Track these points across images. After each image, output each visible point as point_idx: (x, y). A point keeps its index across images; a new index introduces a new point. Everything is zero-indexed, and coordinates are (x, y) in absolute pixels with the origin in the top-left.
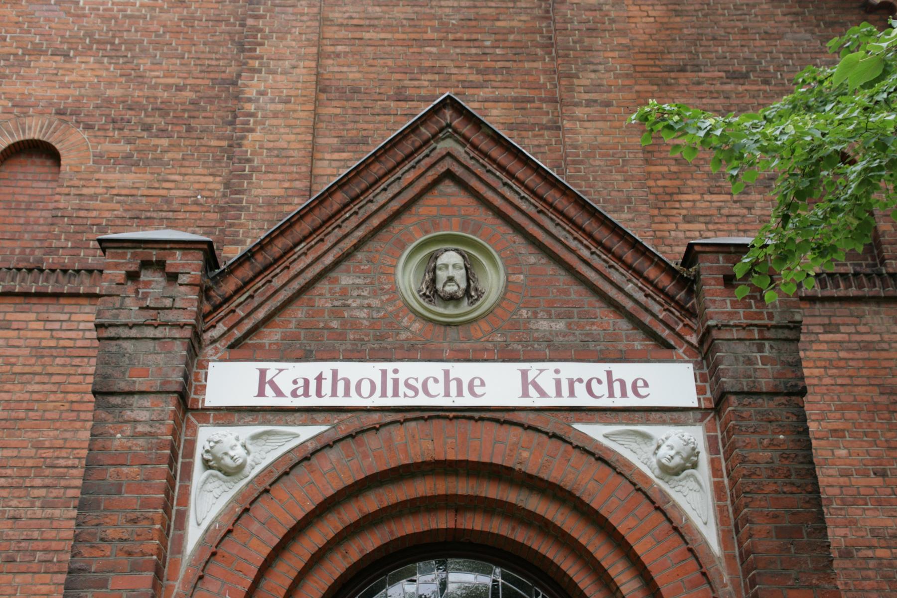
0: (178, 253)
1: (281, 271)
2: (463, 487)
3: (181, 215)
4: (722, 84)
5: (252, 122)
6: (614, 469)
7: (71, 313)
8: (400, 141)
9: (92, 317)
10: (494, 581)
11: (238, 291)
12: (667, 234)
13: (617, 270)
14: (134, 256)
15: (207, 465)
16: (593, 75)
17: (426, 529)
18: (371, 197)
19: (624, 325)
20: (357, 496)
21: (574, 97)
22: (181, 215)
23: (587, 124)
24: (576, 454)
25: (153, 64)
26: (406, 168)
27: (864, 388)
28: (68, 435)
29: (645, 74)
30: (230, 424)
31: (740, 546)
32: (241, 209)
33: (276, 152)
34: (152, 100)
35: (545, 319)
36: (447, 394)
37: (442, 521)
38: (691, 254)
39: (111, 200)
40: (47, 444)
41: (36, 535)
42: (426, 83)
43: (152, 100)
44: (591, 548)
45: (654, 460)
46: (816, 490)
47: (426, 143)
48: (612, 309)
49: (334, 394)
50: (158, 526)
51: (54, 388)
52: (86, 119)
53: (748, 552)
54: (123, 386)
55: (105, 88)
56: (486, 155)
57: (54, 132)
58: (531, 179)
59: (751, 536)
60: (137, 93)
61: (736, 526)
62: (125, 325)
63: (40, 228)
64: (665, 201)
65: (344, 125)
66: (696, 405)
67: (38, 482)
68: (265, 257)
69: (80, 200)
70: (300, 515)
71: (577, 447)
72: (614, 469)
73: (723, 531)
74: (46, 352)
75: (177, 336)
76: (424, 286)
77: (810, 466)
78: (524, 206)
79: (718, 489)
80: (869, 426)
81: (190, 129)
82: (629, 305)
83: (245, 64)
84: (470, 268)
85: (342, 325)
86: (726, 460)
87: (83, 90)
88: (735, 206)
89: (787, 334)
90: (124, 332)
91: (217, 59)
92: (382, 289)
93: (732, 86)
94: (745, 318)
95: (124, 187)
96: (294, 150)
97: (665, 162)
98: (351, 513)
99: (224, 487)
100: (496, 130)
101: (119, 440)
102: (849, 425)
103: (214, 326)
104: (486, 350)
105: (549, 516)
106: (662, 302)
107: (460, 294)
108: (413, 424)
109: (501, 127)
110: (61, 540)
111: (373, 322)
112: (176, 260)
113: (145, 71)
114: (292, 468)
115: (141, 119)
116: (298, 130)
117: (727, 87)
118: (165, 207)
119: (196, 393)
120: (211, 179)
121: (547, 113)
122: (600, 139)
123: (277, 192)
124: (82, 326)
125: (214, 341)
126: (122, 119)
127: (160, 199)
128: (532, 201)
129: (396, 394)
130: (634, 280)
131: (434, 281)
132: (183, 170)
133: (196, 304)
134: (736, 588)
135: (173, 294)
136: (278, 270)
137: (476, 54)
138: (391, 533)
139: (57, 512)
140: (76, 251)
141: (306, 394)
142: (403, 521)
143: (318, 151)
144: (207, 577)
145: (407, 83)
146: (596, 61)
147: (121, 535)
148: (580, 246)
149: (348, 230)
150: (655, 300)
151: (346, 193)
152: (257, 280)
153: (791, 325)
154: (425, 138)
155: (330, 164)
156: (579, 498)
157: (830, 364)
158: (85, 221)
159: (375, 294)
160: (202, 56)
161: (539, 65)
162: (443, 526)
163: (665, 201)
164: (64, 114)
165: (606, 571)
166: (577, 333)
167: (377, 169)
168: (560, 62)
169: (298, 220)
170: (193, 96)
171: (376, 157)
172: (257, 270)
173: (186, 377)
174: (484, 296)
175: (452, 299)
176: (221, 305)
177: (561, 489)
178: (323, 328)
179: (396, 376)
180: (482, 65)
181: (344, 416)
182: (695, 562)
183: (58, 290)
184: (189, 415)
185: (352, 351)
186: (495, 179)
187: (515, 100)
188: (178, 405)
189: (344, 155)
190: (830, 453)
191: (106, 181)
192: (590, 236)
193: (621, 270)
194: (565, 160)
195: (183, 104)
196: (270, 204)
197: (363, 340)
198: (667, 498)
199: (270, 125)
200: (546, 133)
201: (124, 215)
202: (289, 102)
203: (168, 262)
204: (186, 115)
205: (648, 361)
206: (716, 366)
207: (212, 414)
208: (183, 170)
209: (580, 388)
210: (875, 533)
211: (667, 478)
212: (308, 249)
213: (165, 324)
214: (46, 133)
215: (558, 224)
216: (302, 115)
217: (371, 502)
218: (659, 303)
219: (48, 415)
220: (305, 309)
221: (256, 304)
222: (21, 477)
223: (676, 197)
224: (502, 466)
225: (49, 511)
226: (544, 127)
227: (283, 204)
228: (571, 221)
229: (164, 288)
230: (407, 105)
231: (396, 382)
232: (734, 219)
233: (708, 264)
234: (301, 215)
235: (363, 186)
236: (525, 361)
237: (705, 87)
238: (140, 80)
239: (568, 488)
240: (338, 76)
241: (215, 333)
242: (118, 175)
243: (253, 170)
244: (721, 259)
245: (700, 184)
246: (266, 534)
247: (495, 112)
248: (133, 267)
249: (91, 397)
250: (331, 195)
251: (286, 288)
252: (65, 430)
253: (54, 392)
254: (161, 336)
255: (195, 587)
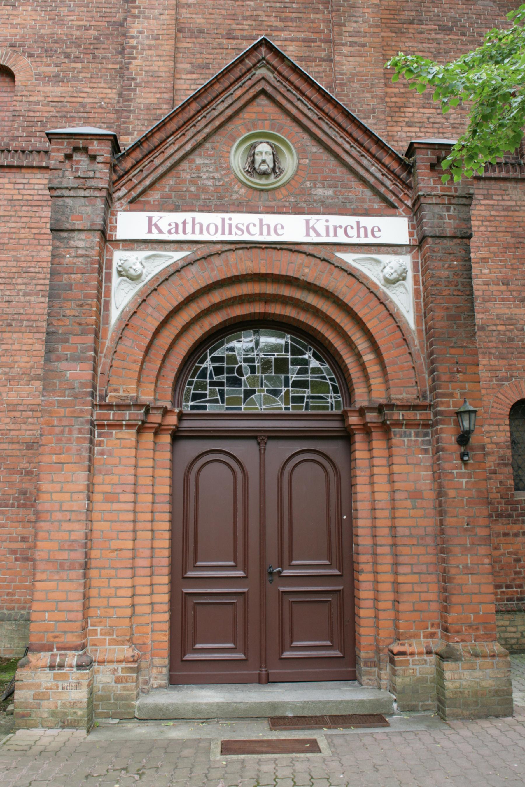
0: (96, 142)
1: (159, 154)
2: (270, 289)
3: (92, 115)
4: (436, 34)
5: (135, 52)
6: (358, 280)
7: (29, 179)
8: (232, 69)
9: (46, 182)
10: (286, 342)
11: (133, 167)
12: (395, 134)
13: (366, 158)
14: (69, 143)
15: (120, 274)
16: (355, 25)
17: (248, 313)
18: (214, 106)
19: (368, 193)
20: (208, 293)
21: (342, 40)
22: (92, 115)
23: (350, 59)
24: (336, 271)
25: (69, 11)
26: (236, 87)
27: (503, 234)
28: (34, 254)
29: (388, 25)
30: (132, 250)
31: (426, 324)
32: (130, 112)
33: (151, 74)
34: (69, 36)
35: (321, 188)
36: (261, 234)
37: (257, 308)
38: (412, 149)
39: (48, 105)
40: (23, 259)
41: (22, 311)
42: (247, 27)
43: (69, 36)
44: (342, 325)
45: (381, 276)
46: (471, 294)
47: (249, 70)
48: (362, 182)
49: (193, 232)
50: (94, 309)
51: (24, 225)
52: (29, 50)
53: (430, 328)
54: (68, 226)
55: (40, 29)
56: (287, 79)
57: (9, 59)
58: (315, 97)
59: (433, 319)
60: (60, 32)
61: (425, 313)
62: (67, 188)
63: (6, 124)
64: (395, 112)
65: (194, 55)
66: (408, 243)
67: (20, 281)
68: (149, 146)
69: (29, 105)
70: (176, 304)
71: (337, 267)
72: (358, 280)
73: (417, 316)
74: (16, 203)
75: (98, 195)
76: (247, 165)
77: (470, 280)
78: (310, 114)
79: (417, 292)
80: (503, 256)
81: (95, 57)
82: (372, 180)
83: (129, 12)
84: (276, 154)
85: (197, 189)
86: (423, 276)
87: (26, 30)
88: (438, 117)
89: (464, 201)
90: (66, 193)
91: (110, 8)
92: (221, 167)
93: (442, 35)
94: (441, 191)
95: (56, 96)
96: (162, 72)
97: (397, 86)
98: (204, 303)
99: (131, 287)
100: (292, 60)
101: (68, 259)
102: (492, 255)
103: (119, 189)
104: (285, 206)
105: (319, 307)
106: (392, 179)
107: (269, 171)
108: (240, 251)
109: (295, 59)
110: (36, 314)
111: (216, 188)
112: (95, 147)
113: (64, 16)
114: (169, 276)
115: (63, 50)
116: (164, 59)
117: (439, 36)
118: (82, 110)
119: (111, 231)
120: (109, 91)
121: (324, 50)
122: (358, 69)
123: (153, 100)
124: (36, 187)
125: (120, 199)
126: (51, 50)
127: (78, 105)
128: (316, 111)
129: (230, 233)
130: (376, 165)
131: (253, 162)
132: (92, 85)
133: (108, 175)
134: (422, 347)
135: (94, 169)
136: (157, 154)
137: (280, 7)
138: (228, 314)
139: (32, 299)
140: (29, 139)
141: (177, 232)
142: (235, 307)
143: (177, 73)
144: (124, 338)
145: (234, 26)
146: (358, 15)
147: (74, 314)
148: (344, 142)
149: (200, 128)
150: (388, 177)
151: (198, 103)
152: (145, 160)
153: (468, 196)
154: (248, 67)
155: (185, 82)
156: (337, 297)
157: (485, 219)
158: (33, 119)
159: (217, 170)
160: (101, 5)
161: (320, 16)
162: (258, 311)
163: (395, 112)
164: (15, 46)
165: (350, 337)
166: (340, 197)
167: (218, 88)
168: (334, 14)
169: (169, 121)
170: (96, 33)
171: (217, 79)
172: (145, 153)
173: (105, 221)
174: (284, 173)
175: (265, 174)
176: (123, 176)
177: (327, 291)
178: (186, 191)
179: (230, 222)
180: (283, 15)
181: (199, 246)
182: (400, 333)
183: (20, 164)
184: (108, 244)
185: (203, 206)
186: (293, 96)
187: (304, 40)
188: (101, 238)
189: (194, 76)
190: (479, 271)
191: (44, 92)
192: (350, 135)
193: (369, 158)
194: (335, 83)
195: (89, 39)
196: (148, 109)
197: (210, 199)
198: (387, 297)
199: (146, 55)
200: (323, 64)
201: (57, 115)
202: (158, 39)
203: (90, 148)
204: (92, 47)
205: (381, 216)
206: (421, 220)
207: (121, 243)
208: (92, 85)
209: (340, 232)
210: (498, 317)
211: (388, 285)
212: (176, 140)
213: (90, 188)
214: (5, 59)
215: (331, 127)
216: (167, 48)
217: (216, 297)
218: (390, 180)
219: (21, 242)
220: (174, 179)
221: (144, 176)
222: (10, 278)
223: (402, 110)
224: (293, 277)
225: (28, 298)
226: (322, 60)
227: (156, 109)
228: (339, 125)
229: (88, 164)
230: (235, 42)
231: (230, 226)
232: (437, 126)
233: (421, 156)
234: (171, 118)
235: (209, 99)
236: (308, 214)
237: (425, 35)
238: (61, 22)
239: (331, 291)
240: (190, 21)
241: (120, 194)
242: (51, 88)
243: (137, 85)
244: (429, 153)
245: (418, 101)
246: (156, 315)
247: (291, 48)
248: (69, 152)
249: (49, 231)
250: (189, 104)
251: (162, 165)
252: (32, 251)
253: (24, 228)
254: (88, 195)
255: (117, 343)
